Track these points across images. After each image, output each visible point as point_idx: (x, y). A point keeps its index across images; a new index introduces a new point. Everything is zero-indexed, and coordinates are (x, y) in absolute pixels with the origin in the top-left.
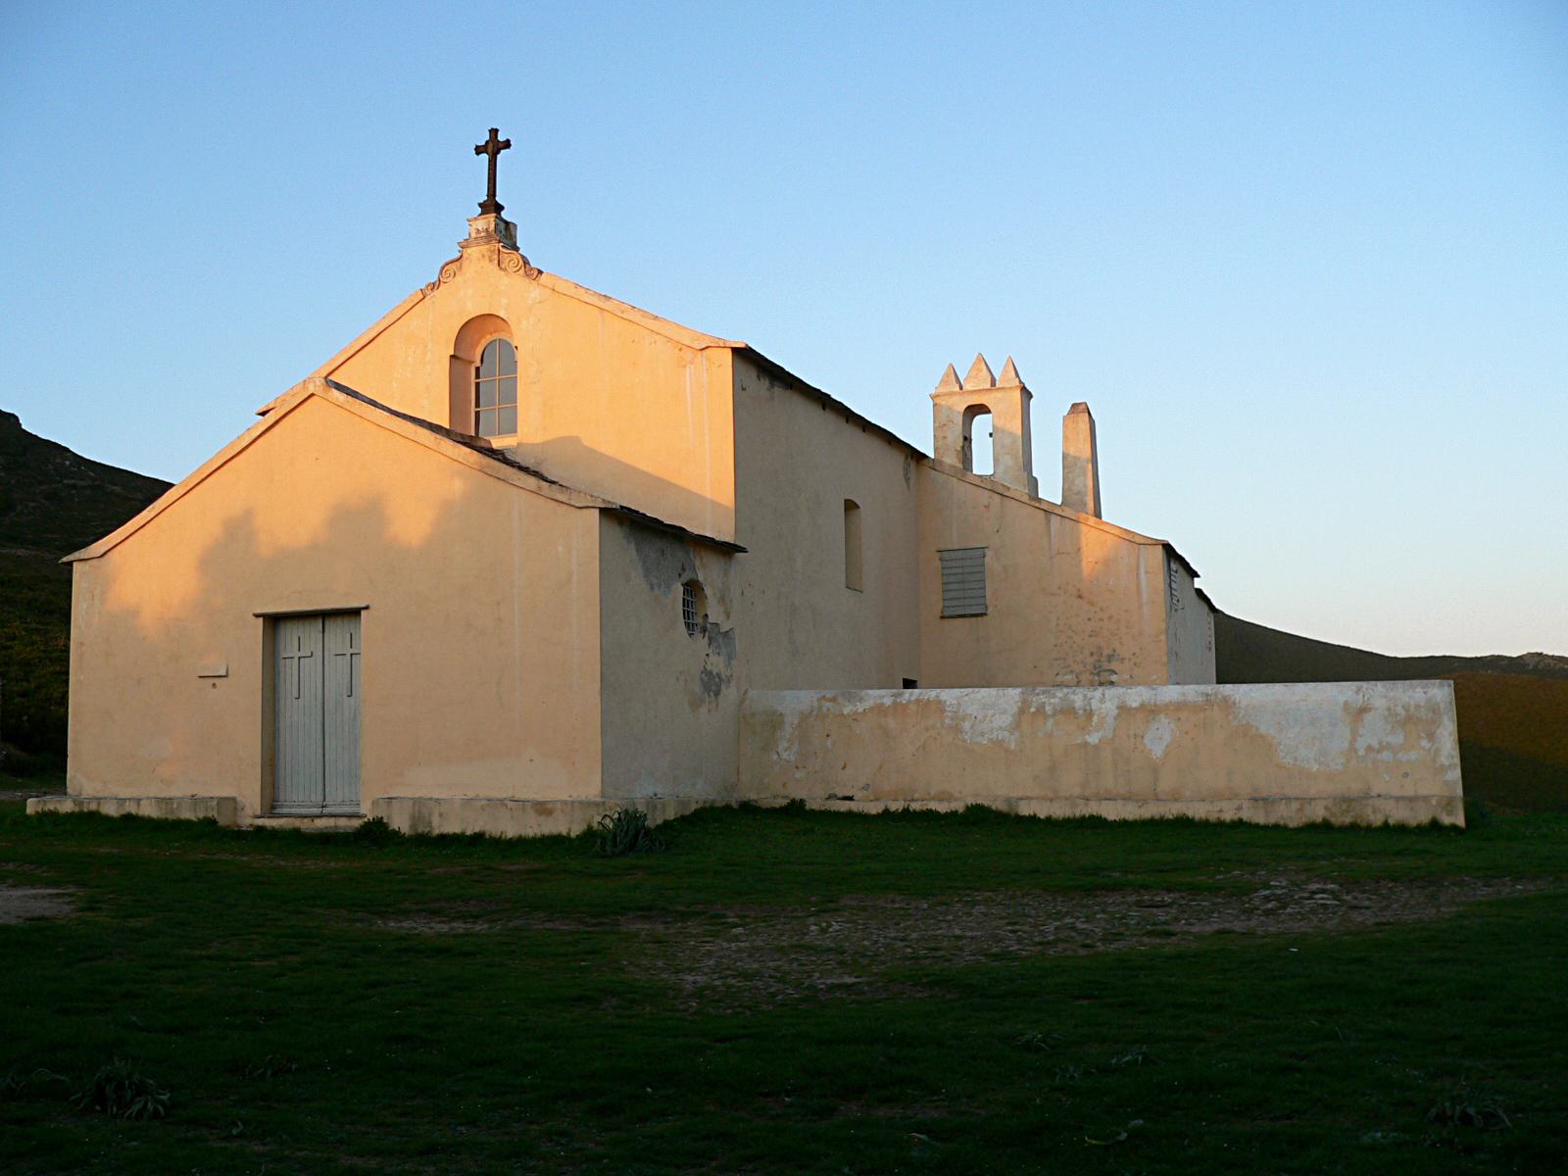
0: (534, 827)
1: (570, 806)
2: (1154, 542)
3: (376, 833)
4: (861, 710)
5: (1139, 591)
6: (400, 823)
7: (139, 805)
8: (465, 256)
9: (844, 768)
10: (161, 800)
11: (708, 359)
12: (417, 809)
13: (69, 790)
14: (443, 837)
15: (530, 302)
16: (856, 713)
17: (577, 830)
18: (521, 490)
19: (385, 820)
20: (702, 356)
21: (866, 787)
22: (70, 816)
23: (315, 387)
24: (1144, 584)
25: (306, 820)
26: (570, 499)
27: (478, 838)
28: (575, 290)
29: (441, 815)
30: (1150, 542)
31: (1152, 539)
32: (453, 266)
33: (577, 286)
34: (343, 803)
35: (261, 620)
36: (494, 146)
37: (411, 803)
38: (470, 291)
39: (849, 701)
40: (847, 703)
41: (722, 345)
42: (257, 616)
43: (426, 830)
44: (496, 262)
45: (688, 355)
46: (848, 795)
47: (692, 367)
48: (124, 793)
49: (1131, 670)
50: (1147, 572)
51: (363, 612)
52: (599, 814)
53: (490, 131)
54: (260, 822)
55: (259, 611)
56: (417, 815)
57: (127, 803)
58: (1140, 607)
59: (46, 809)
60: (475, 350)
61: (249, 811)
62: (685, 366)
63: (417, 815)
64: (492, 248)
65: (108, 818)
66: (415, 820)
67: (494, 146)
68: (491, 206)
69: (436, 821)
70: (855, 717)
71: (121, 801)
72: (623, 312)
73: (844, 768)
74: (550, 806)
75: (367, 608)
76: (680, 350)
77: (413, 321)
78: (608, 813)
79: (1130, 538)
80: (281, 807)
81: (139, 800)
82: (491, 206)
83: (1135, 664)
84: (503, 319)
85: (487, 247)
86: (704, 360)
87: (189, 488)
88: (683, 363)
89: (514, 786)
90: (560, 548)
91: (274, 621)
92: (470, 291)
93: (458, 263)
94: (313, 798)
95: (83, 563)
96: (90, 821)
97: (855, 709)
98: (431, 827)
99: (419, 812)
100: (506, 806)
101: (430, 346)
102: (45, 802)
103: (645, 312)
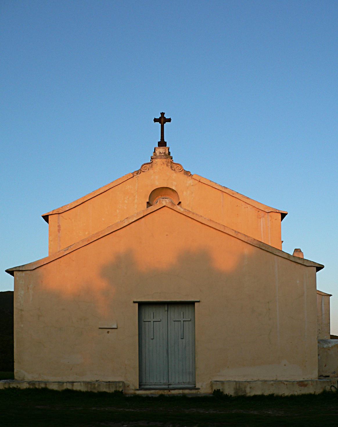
0: (298, 391)
1: (315, 383)
2: (327, 295)
3: (218, 396)
4: (330, 346)
5: (321, 310)
6: (229, 391)
7: (73, 385)
8: (154, 162)
9: (325, 366)
10: (87, 383)
11: (271, 216)
12: (238, 385)
13: (16, 378)
14: (255, 396)
15: (188, 185)
16: (329, 347)
17: (319, 391)
18: (279, 257)
19: (221, 391)
20: (268, 215)
21: (334, 373)
22: (28, 390)
23: (166, 203)
24: (323, 308)
25: (165, 391)
26: (304, 262)
27: (271, 397)
28: (210, 183)
29: (251, 388)
30: (326, 295)
31: (327, 294)
32: (148, 166)
33: (211, 181)
34: (179, 383)
35: (137, 304)
36: (162, 120)
37: (235, 383)
38: (157, 177)
39: (325, 343)
40: (325, 344)
41: (278, 212)
42: (134, 302)
43: (244, 394)
44: (170, 167)
45: (262, 214)
46: (327, 375)
47: (264, 218)
48: (59, 379)
49: (318, 335)
50: (324, 304)
51: (196, 304)
52: (329, 385)
53: (161, 113)
54: (138, 392)
55: (135, 300)
56: (238, 388)
57: (65, 384)
58: (322, 315)
59: (11, 386)
60: (154, 201)
61: (132, 387)
62: (261, 218)
63: (238, 388)
64: (168, 161)
65: (52, 391)
66: (237, 390)
67: (162, 120)
68: (162, 143)
69: (248, 390)
70: (329, 349)
71: (61, 383)
72: (233, 194)
73: (325, 366)
74: (306, 383)
75: (199, 302)
76: (258, 211)
77: (128, 186)
78: (332, 385)
79: (319, 293)
80: (145, 385)
81: (73, 383)
82: (162, 143)
83: (319, 333)
84: (173, 190)
85: (165, 160)
86: (269, 217)
87: (89, 242)
88: (260, 217)
89: (276, 375)
90: (298, 282)
91: (142, 305)
92: (157, 177)
93: (150, 165)
94: (162, 381)
95: (20, 272)
96: (40, 394)
97: (328, 346)
98: (245, 392)
99: (239, 387)
100: (284, 384)
101: (136, 197)
102: (9, 383)
103: (243, 195)
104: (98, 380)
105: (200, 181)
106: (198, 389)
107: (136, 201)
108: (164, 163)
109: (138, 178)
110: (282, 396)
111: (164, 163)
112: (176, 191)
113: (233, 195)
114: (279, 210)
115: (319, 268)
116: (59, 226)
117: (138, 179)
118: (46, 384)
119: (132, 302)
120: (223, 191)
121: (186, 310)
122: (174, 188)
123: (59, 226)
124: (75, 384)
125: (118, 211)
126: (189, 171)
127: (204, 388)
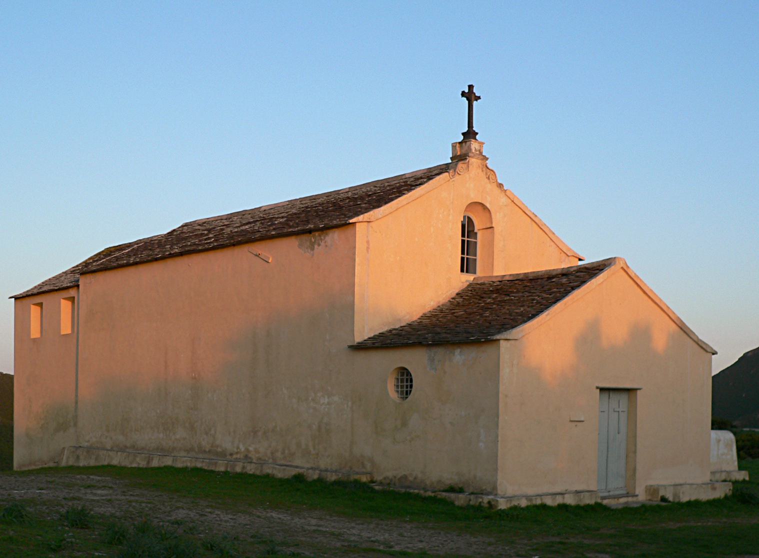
104: (566, 489)
105: (513, 201)
106: (637, 496)
107: (451, 217)
108: (479, 167)
109: (453, 182)
110: (482, 507)
111: (479, 167)
112: (489, 211)
113: (540, 226)
114: (576, 253)
115: (715, 353)
116: (368, 242)
117: (453, 185)
118: (531, 500)
119: (595, 387)
120: (533, 219)
121: (611, 396)
122: (488, 206)
123: (368, 242)
124: (566, 496)
125: (432, 230)
126: (502, 183)
127: (642, 496)
